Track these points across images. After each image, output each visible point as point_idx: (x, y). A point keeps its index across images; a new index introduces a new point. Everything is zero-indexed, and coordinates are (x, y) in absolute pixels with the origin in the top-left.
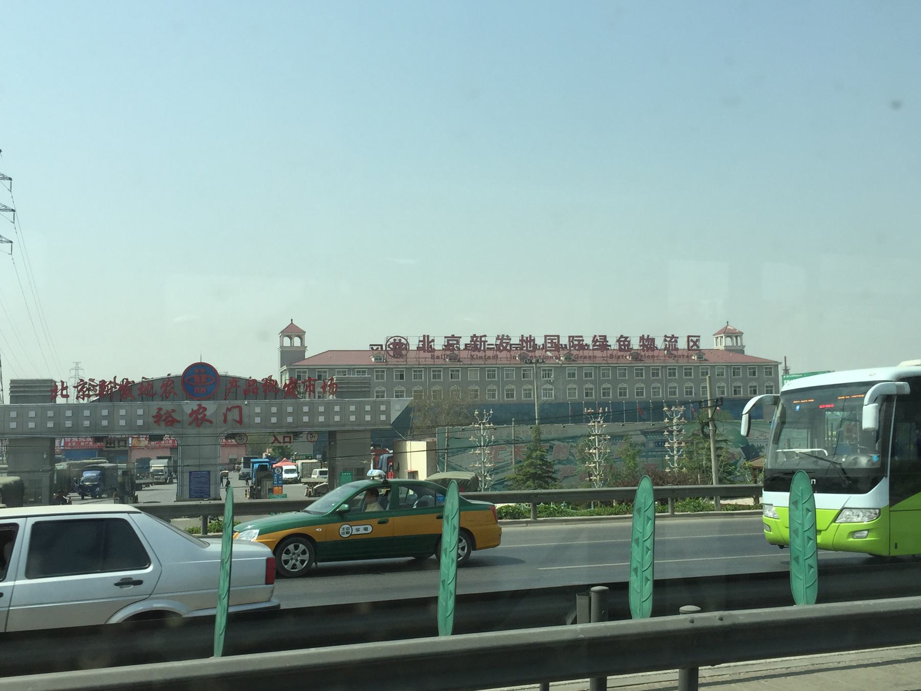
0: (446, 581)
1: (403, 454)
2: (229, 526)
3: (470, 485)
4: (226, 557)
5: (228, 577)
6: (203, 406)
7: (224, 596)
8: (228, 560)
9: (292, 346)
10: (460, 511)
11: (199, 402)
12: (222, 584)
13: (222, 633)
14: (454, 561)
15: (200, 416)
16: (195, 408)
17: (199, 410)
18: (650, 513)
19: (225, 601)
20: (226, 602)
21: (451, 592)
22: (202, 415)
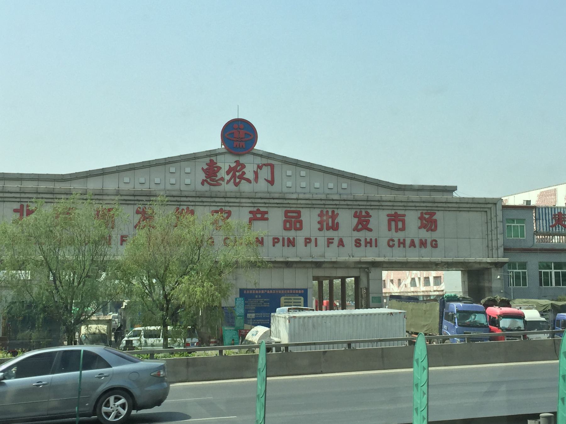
0: (419, 408)
1: (82, 381)
2: (263, 370)
3: (208, 329)
4: (261, 393)
5: (264, 407)
6: (241, 162)
7: (261, 421)
8: (263, 396)
9: (278, 293)
10: (428, 355)
11: (237, 158)
12: (259, 413)
13: (264, 368)
14: (425, 394)
15: (238, 174)
16: (233, 165)
17: (236, 167)
18: (425, 363)
19: (264, 372)
20: (265, 373)
21: (423, 417)
22: (241, 173)
